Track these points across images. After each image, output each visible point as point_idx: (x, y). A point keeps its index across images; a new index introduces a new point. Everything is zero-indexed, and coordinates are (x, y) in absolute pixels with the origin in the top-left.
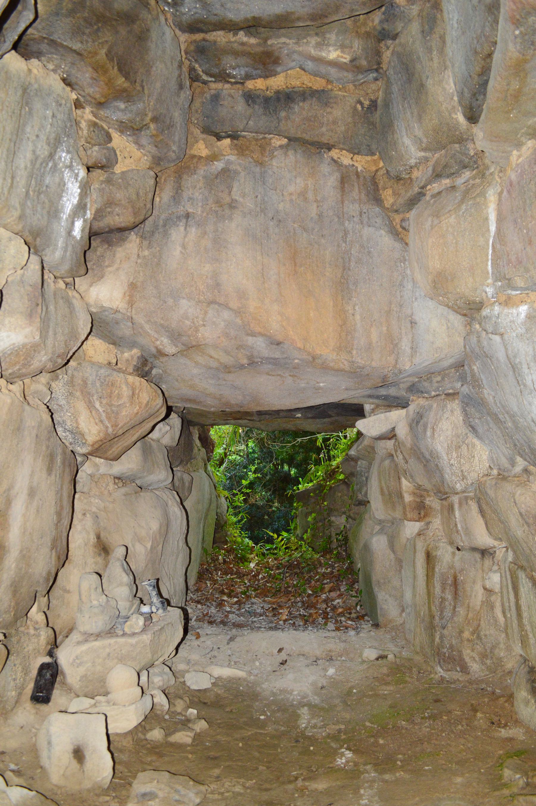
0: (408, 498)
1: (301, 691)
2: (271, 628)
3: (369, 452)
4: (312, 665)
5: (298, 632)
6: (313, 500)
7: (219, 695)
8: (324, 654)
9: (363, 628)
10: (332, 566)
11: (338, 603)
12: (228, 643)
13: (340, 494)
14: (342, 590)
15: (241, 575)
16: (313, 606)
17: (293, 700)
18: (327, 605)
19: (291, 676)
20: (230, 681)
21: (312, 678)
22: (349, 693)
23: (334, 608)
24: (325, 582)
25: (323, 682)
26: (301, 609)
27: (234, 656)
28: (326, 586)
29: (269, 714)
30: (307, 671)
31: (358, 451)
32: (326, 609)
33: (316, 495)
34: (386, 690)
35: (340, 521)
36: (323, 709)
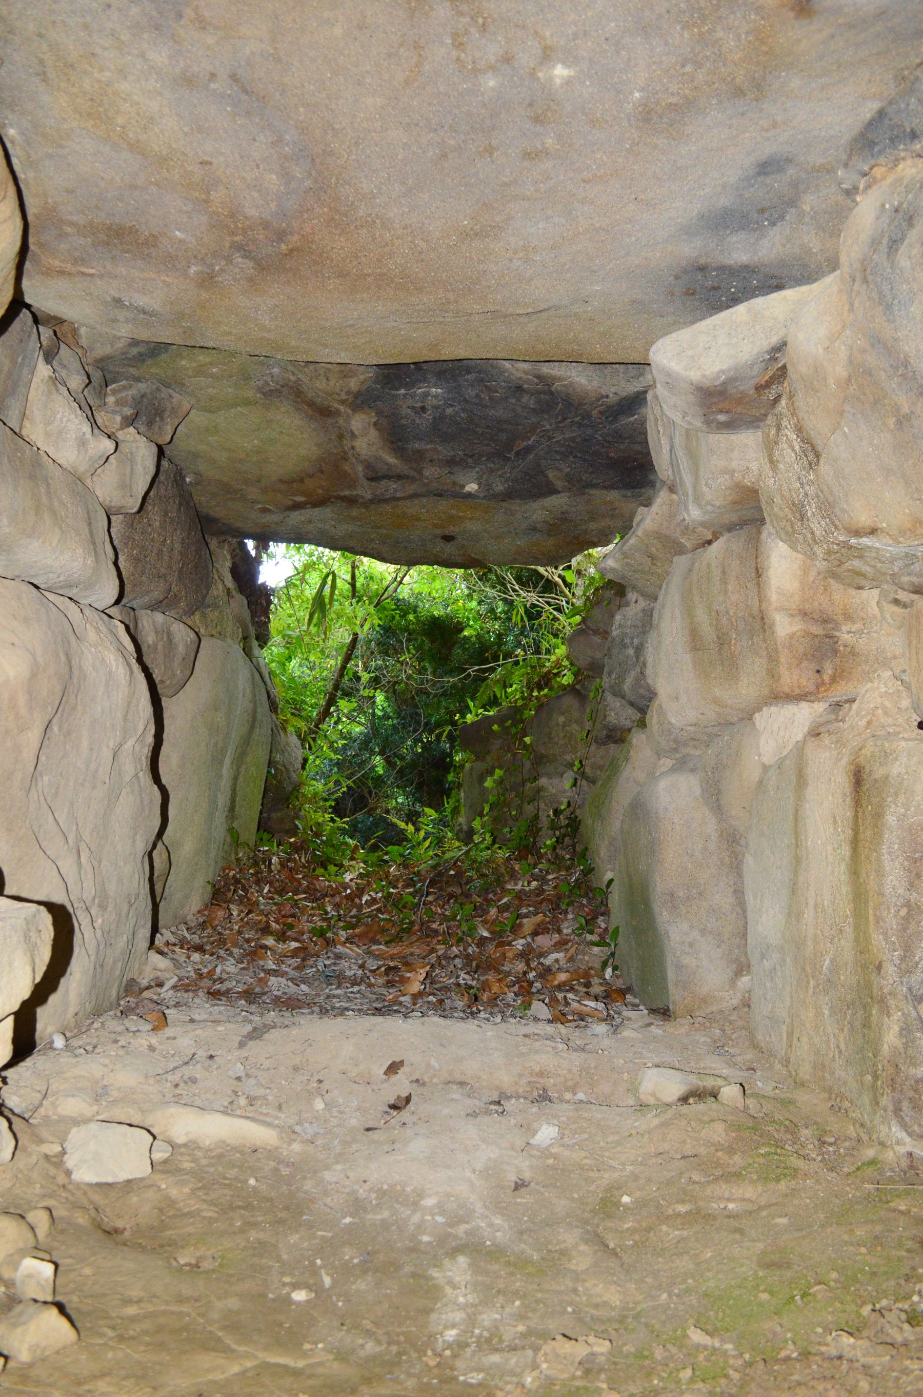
0: (785, 627)
1: (448, 1195)
2: (378, 1011)
3: (652, 557)
4: (488, 1113)
5: (448, 1022)
6: (496, 744)
7: (172, 1203)
8: (523, 1081)
9: (629, 1019)
10: (543, 880)
11: (557, 961)
12: (242, 1045)
13: (561, 719)
14: (565, 931)
15: (316, 896)
16: (492, 965)
17: (420, 1226)
18: (528, 965)
19: (419, 1146)
20: (221, 1156)
21: (487, 1154)
22: (608, 1206)
23: (546, 973)
24: (524, 910)
25: (524, 1167)
26: (462, 975)
27: (252, 1081)
28: (525, 921)
29: (327, 1281)
30: (470, 1131)
31: (625, 555)
32: (525, 973)
33: (506, 730)
34: (734, 1197)
35: (559, 787)
36: (520, 1264)
